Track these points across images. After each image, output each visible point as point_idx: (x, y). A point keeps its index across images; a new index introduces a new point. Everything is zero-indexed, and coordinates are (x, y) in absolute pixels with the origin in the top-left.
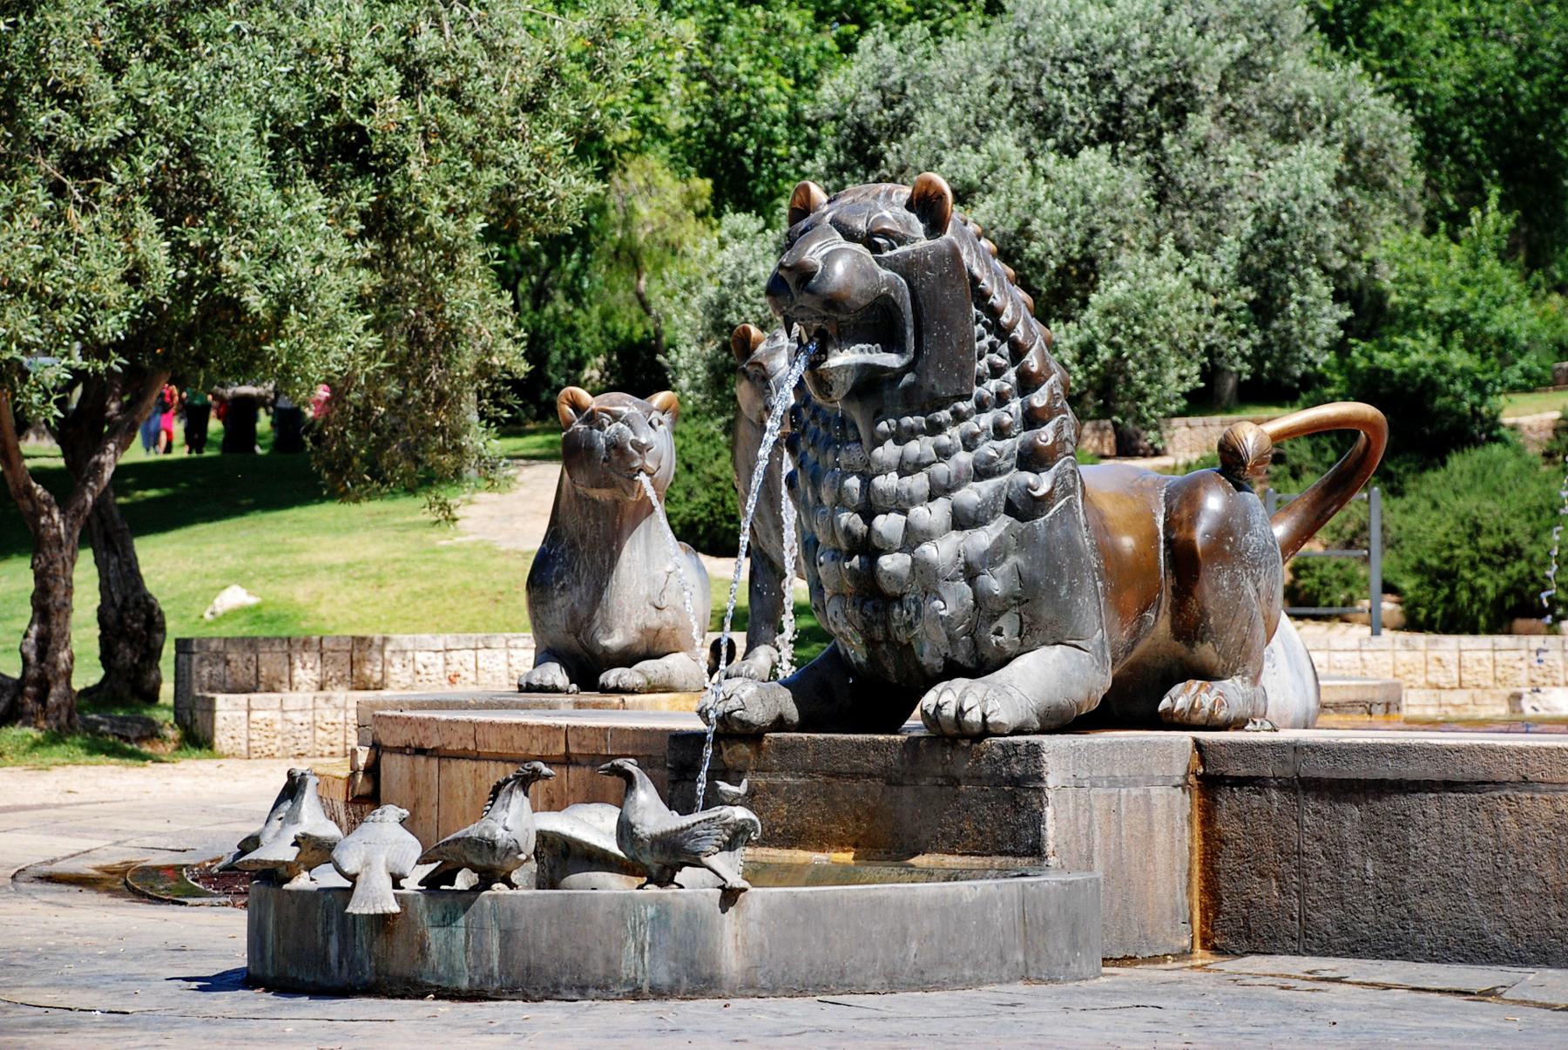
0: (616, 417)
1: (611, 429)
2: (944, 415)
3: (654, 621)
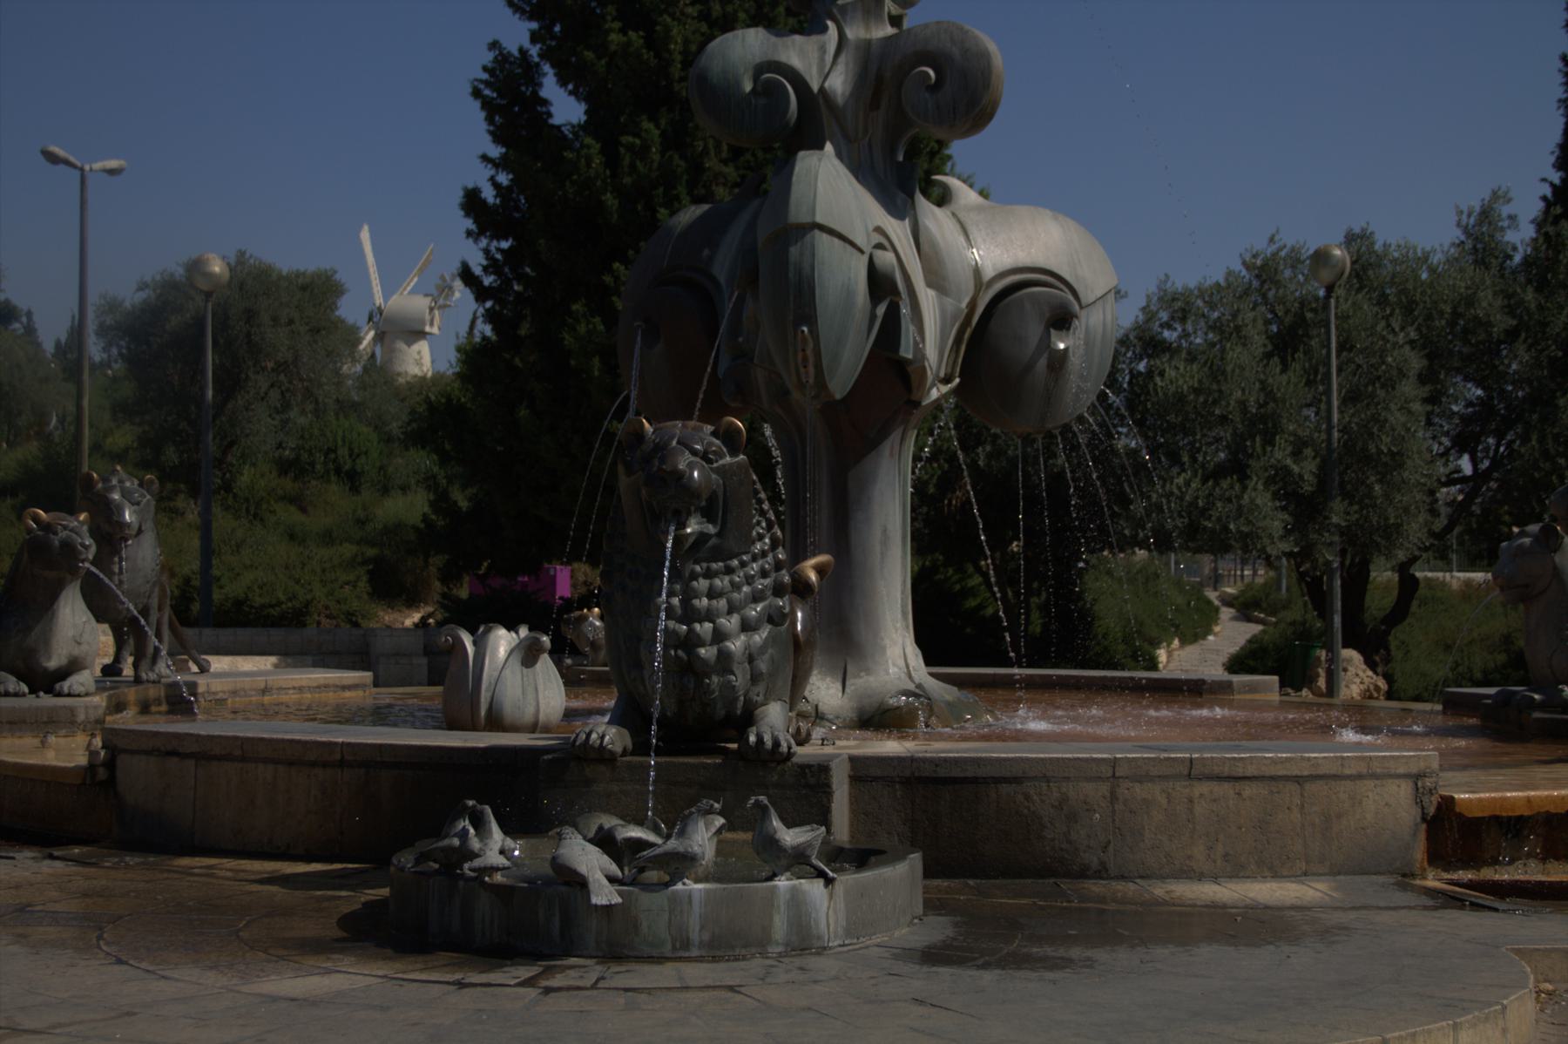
0: (65, 528)
1: (63, 534)
2: (735, 562)
3: (76, 652)
